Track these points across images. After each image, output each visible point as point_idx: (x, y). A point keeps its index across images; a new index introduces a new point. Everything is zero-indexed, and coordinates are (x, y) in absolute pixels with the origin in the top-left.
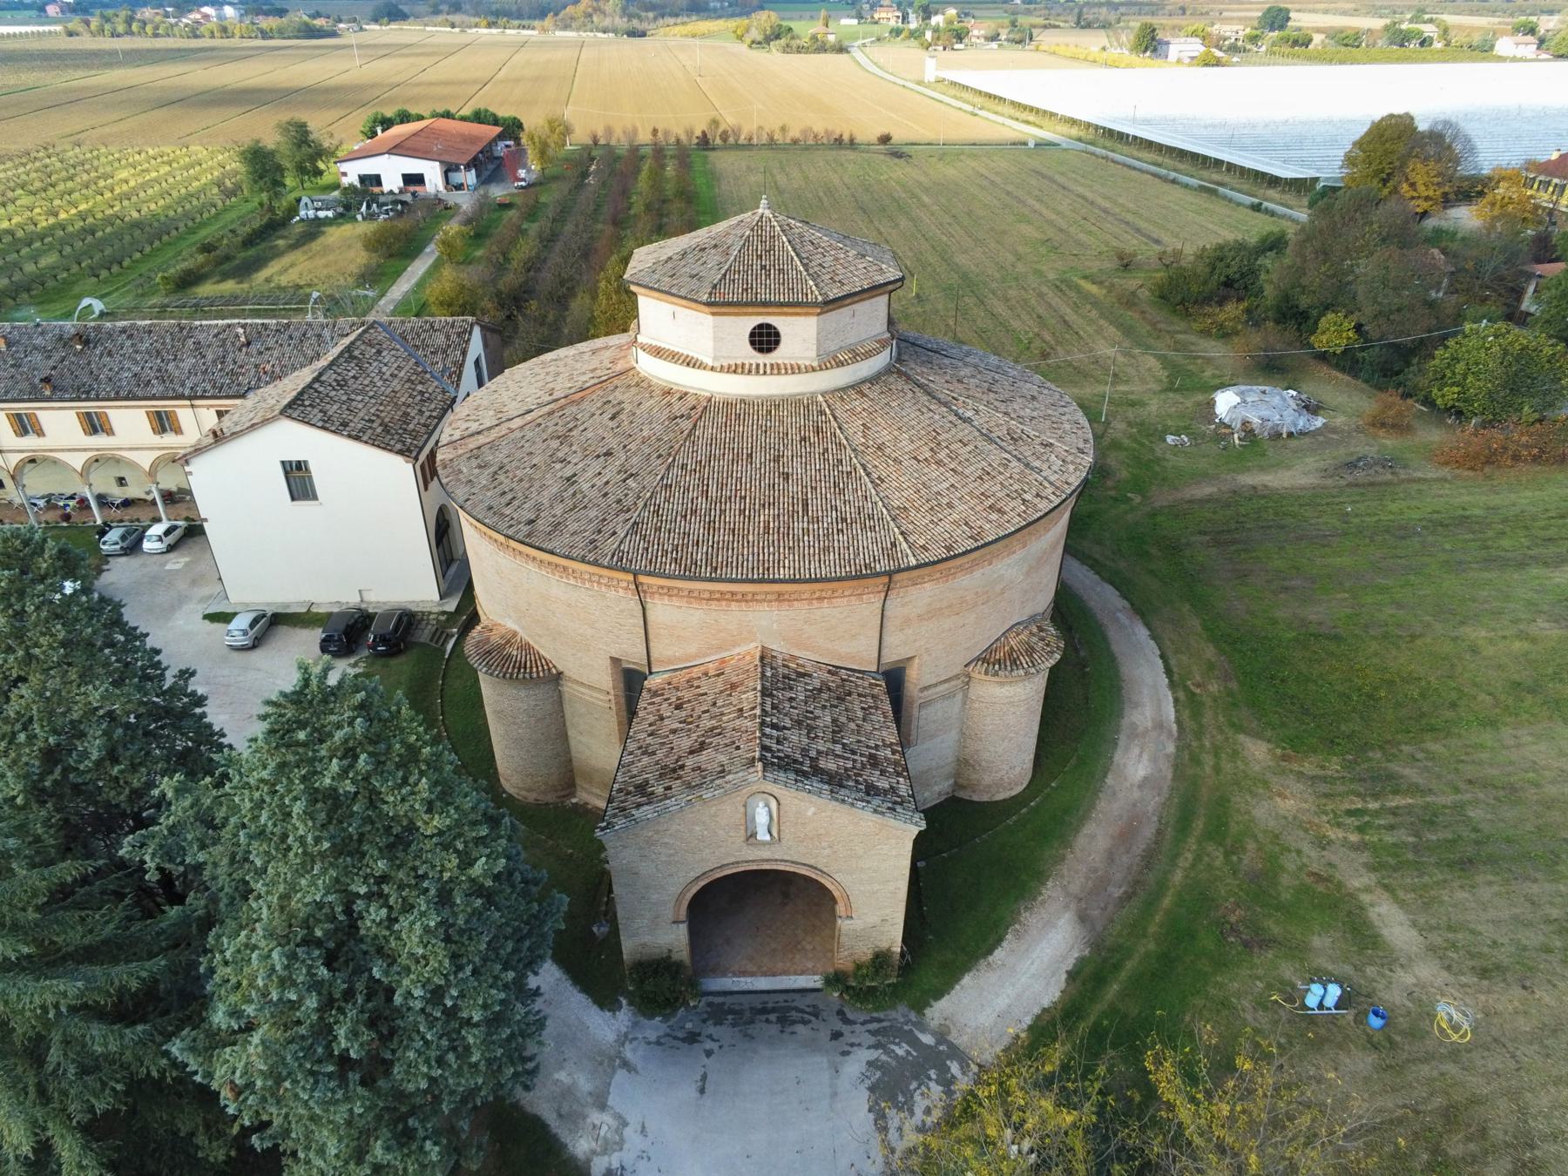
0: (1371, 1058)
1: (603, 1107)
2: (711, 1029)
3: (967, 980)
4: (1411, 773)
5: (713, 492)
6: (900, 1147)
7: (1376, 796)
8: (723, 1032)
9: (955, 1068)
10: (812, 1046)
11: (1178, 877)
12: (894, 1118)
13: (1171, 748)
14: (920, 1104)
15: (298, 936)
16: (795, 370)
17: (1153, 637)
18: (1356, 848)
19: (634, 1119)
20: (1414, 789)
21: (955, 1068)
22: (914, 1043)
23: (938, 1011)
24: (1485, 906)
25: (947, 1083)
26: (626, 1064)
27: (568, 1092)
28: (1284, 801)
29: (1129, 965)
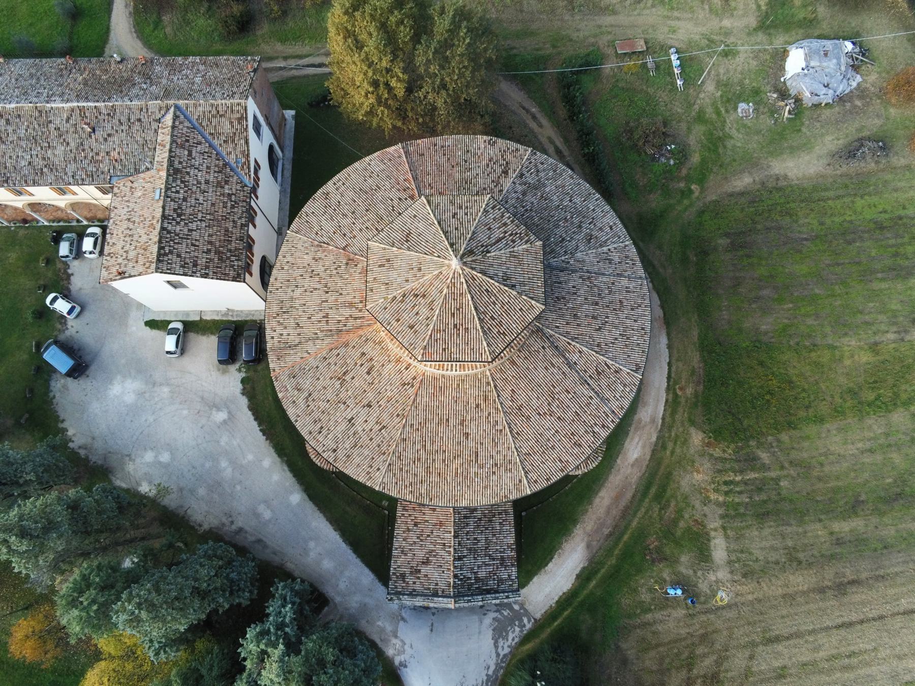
1: (396, 637)
3: (535, 579)
4: (764, 456)
6: (502, 653)
7: (741, 472)
9: (525, 620)
11: (634, 524)
13: (654, 439)
14: (511, 636)
17: (669, 347)
18: (718, 504)
19: (408, 642)
20: (764, 468)
21: (525, 620)
24: (762, 541)
25: (522, 626)
26: (403, 619)
27: (382, 630)
28: (698, 475)
29: (603, 571)
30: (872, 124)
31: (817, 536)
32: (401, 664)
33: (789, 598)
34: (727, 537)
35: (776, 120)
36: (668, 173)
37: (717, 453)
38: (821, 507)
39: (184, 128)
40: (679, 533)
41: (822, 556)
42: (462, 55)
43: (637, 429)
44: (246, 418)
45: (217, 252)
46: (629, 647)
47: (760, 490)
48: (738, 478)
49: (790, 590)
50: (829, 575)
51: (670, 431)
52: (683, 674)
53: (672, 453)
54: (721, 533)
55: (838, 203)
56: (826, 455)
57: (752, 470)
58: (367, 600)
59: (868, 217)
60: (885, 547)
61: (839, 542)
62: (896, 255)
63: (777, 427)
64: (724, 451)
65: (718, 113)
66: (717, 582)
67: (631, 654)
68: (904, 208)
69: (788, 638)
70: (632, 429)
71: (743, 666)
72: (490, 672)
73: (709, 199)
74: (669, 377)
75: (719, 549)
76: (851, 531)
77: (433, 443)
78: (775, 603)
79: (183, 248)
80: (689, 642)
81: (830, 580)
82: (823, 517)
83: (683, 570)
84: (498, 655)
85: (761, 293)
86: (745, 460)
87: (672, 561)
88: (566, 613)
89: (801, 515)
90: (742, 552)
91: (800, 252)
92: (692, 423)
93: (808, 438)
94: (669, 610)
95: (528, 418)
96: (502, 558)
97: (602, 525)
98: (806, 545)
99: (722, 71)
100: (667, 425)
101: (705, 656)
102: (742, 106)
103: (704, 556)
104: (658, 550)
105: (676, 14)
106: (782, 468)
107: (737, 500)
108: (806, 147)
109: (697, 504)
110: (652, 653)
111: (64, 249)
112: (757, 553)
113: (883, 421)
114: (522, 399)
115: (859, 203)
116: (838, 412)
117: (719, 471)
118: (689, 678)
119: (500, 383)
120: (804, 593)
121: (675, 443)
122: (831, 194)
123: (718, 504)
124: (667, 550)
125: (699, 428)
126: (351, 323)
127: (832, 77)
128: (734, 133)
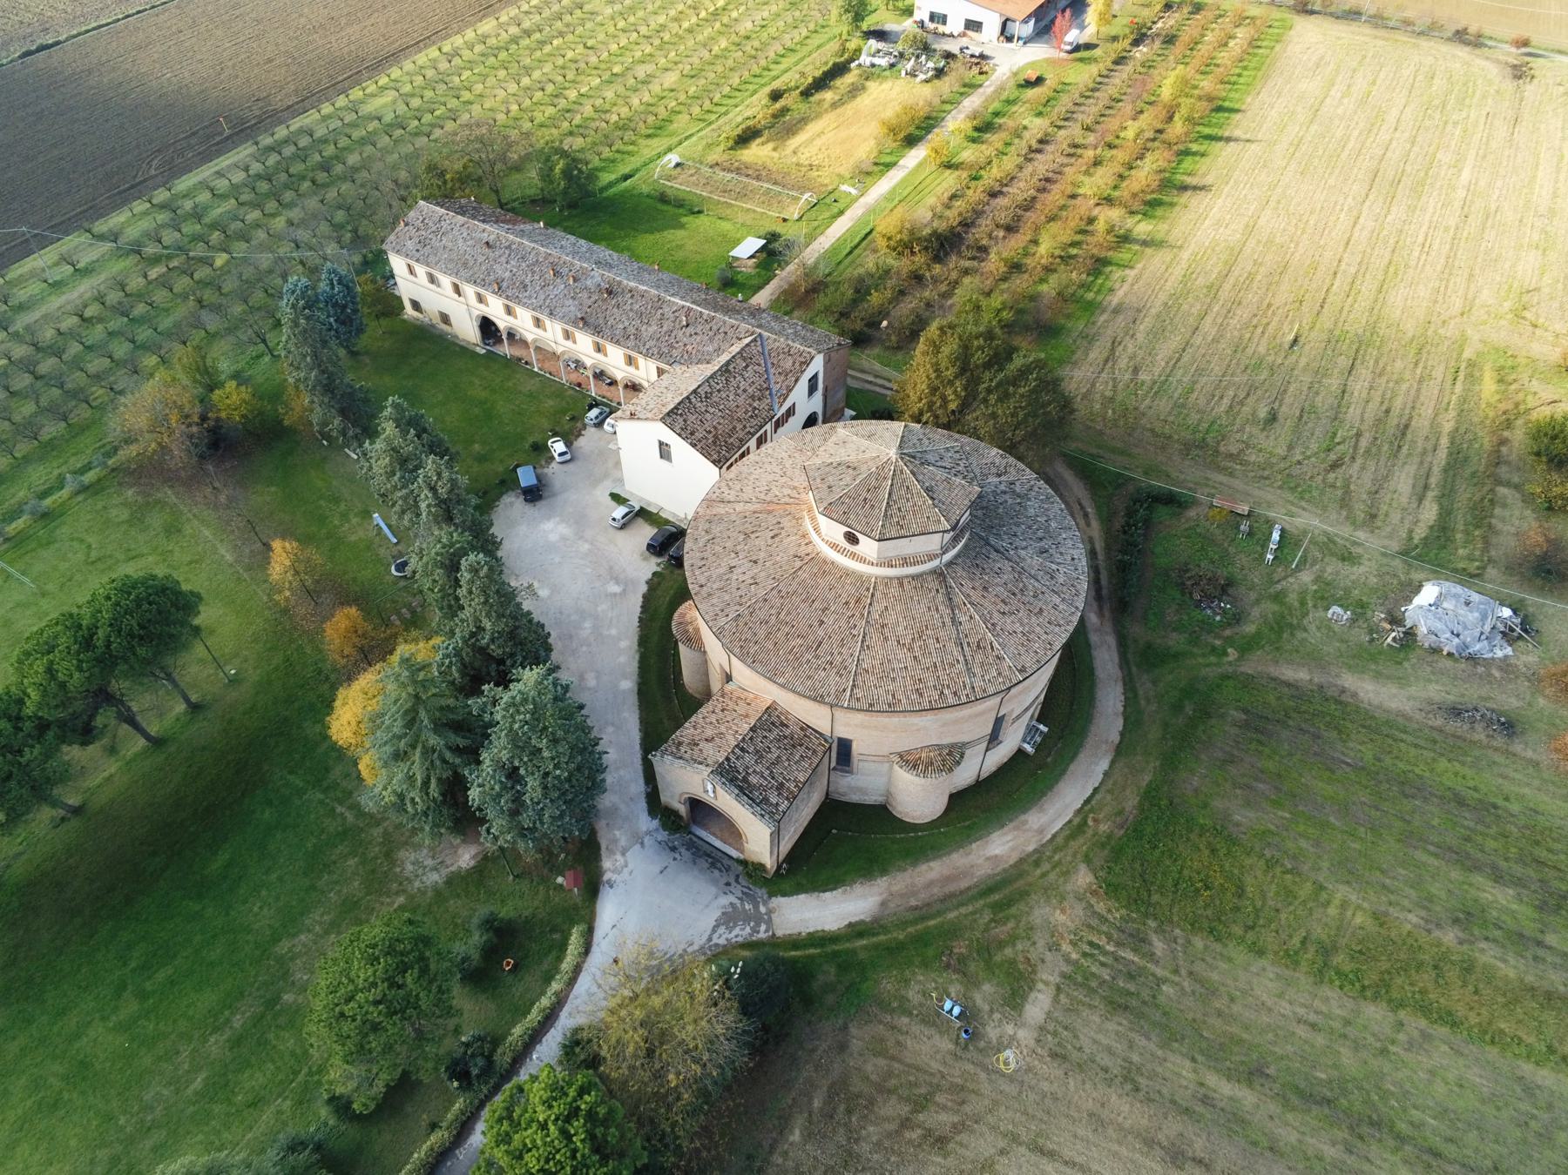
0: (951, 1046)
1: (623, 854)
2: (683, 850)
3: (802, 896)
4: (1159, 946)
5: (782, 616)
6: (715, 940)
7: (1119, 944)
8: (687, 854)
9: (763, 927)
10: (715, 882)
11: (951, 915)
12: (722, 930)
13: (1031, 848)
14: (737, 931)
15: (499, 765)
16: (863, 560)
17: (1106, 774)
18: (1068, 960)
19: (631, 866)
20: (1151, 956)
21: (763, 927)
22: (756, 907)
23: (778, 901)
24: (1099, 1032)
25: (755, 931)
26: (642, 844)
27: (615, 841)
28: (1063, 917)
29: (882, 938)
30: (1508, 700)
31: (1179, 1075)
32: (609, 882)
33: (1097, 1121)
34: (1056, 1000)
35: (1372, 640)
36: (1207, 627)
37: (1100, 907)
38: (1204, 1045)
39: (754, 350)
40: (998, 958)
41: (1173, 1102)
42: (1022, 396)
43: (1016, 828)
44: (635, 603)
45: (716, 437)
46: (859, 1035)
47: (1131, 977)
48: (1110, 948)
49: (1105, 1114)
50: (1172, 1128)
51: (1055, 852)
52: (905, 1110)
53: (1044, 875)
54: (1052, 990)
55: (1413, 751)
56: (1244, 993)
57: (1135, 950)
58: (622, 806)
59: (1449, 784)
60: (1271, 1149)
61: (1206, 1100)
62: (1467, 839)
63: (1194, 925)
64: (1109, 911)
65: (1303, 603)
66: (1013, 1038)
67: (856, 1045)
68: (1507, 799)
69: (1066, 1163)
70: (1011, 825)
71: (987, 1154)
72: (690, 950)
73: (1242, 669)
74: (1087, 801)
75: (1038, 1006)
76: (1231, 1098)
77: (789, 613)
78: (1076, 1115)
79: (692, 418)
80: (935, 1081)
81: (1167, 1137)
82: (1200, 1058)
83: (978, 999)
84: (710, 939)
85: (1254, 784)
86: (1131, 935)
87: (971, 982)
88: (812, 951)
89: (1170, 1037)
90: (1066, 1028)
91: (1333, 772)
92: (1087, 860)
93: (1230, 960)
94: (933, 1031)
95: (886, 639)
96: (782, 784)
97: (914, 894)
98: (1156, 1075)
99: (1329, 570)
100: (1058, 843)
101: (944, 1108)
102: (1336, 609)
103: (1015, 999)
104: (962, 960)
105: (1303, 504)
106: (1176, 971)
107: (1094, 969)
108: (1402, 681)
109: (1041, 943)
110: (882, 1062)
111: (594, 412)
112: (1085, 1042)
113: (1350, 1004)
114: (891, 618)
115: (1443, 764)
116: (1291, 958)
117: (1089, 926)
118: (907, 1119)
119: (878, 594)
120: (1120, 1128)
121: (1054, 868)
122: (1409, 739)
123: (1068, 960)
124: (972, 967)
125: (1094, 872)
126: (787, 500)
127: (1465, 628)
128: (1312, 628)
